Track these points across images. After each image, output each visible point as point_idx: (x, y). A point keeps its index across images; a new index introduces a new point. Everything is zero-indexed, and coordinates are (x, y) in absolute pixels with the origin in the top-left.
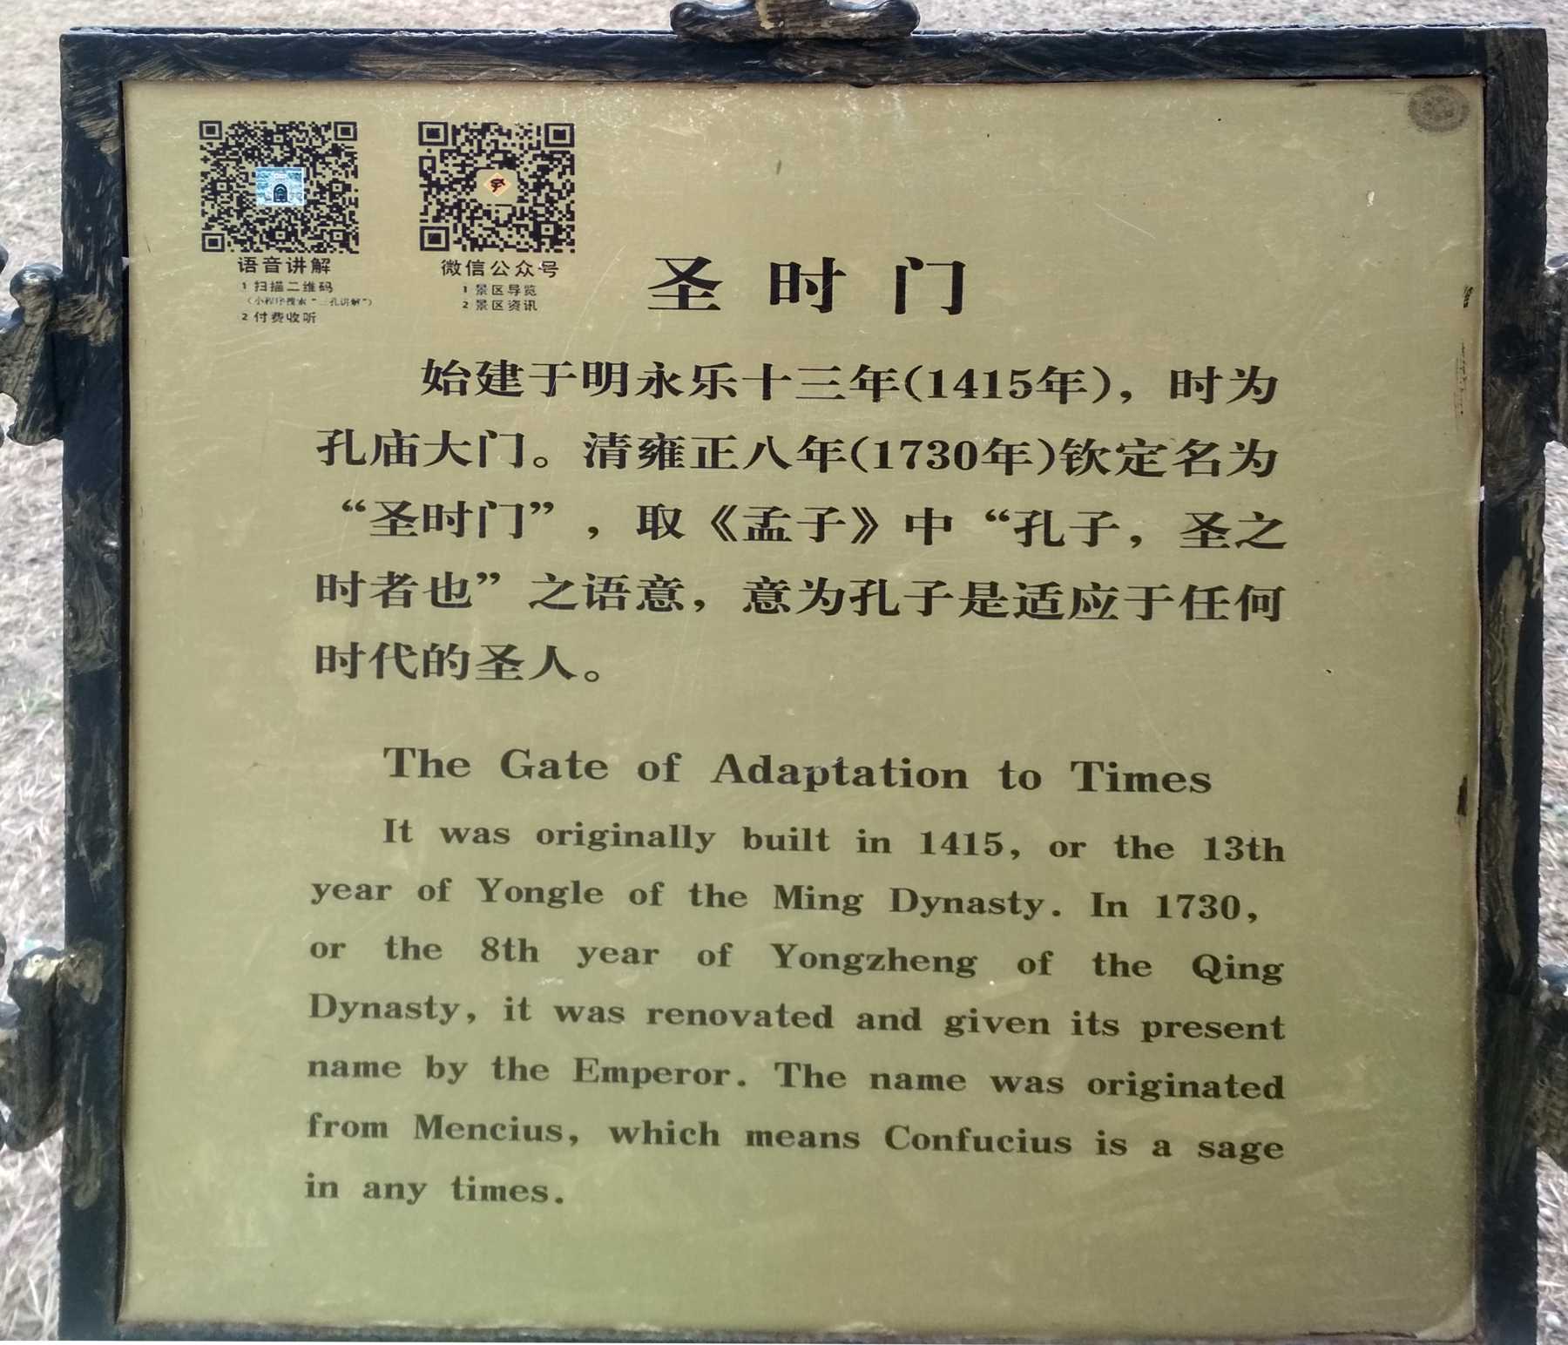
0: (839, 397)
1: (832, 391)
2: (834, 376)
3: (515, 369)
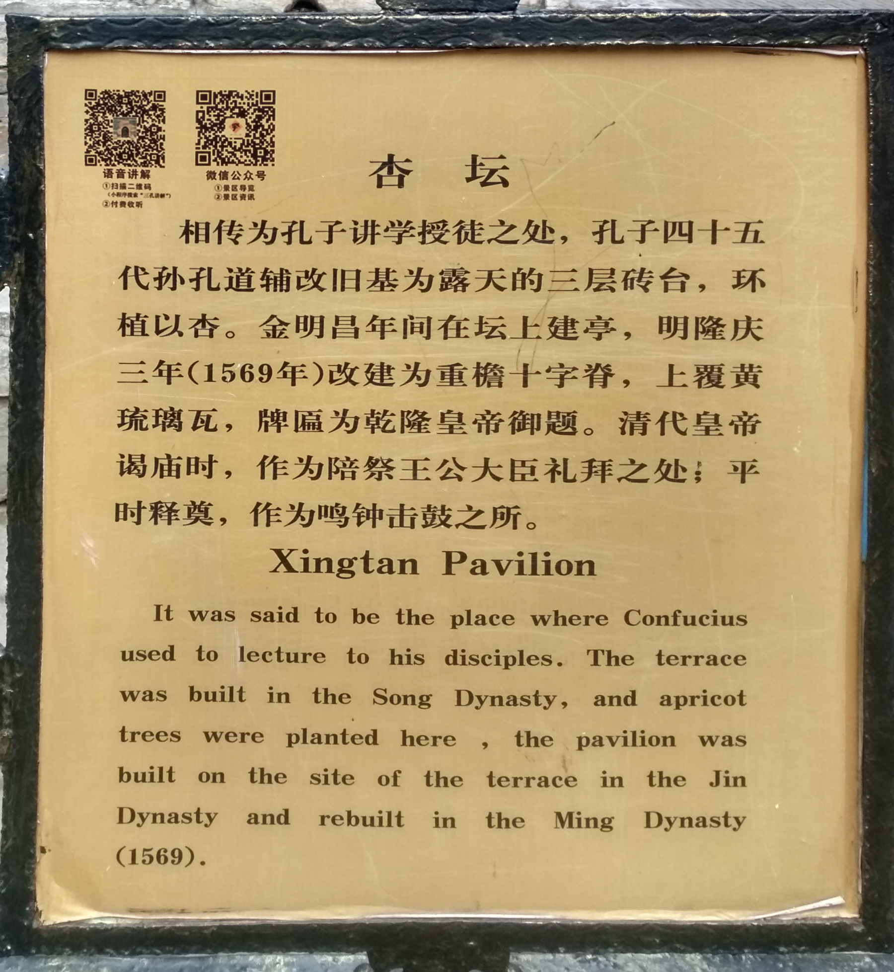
0: (145, 381)
1: (141, 377)
2: (141, 367)
3: (573, 322)
